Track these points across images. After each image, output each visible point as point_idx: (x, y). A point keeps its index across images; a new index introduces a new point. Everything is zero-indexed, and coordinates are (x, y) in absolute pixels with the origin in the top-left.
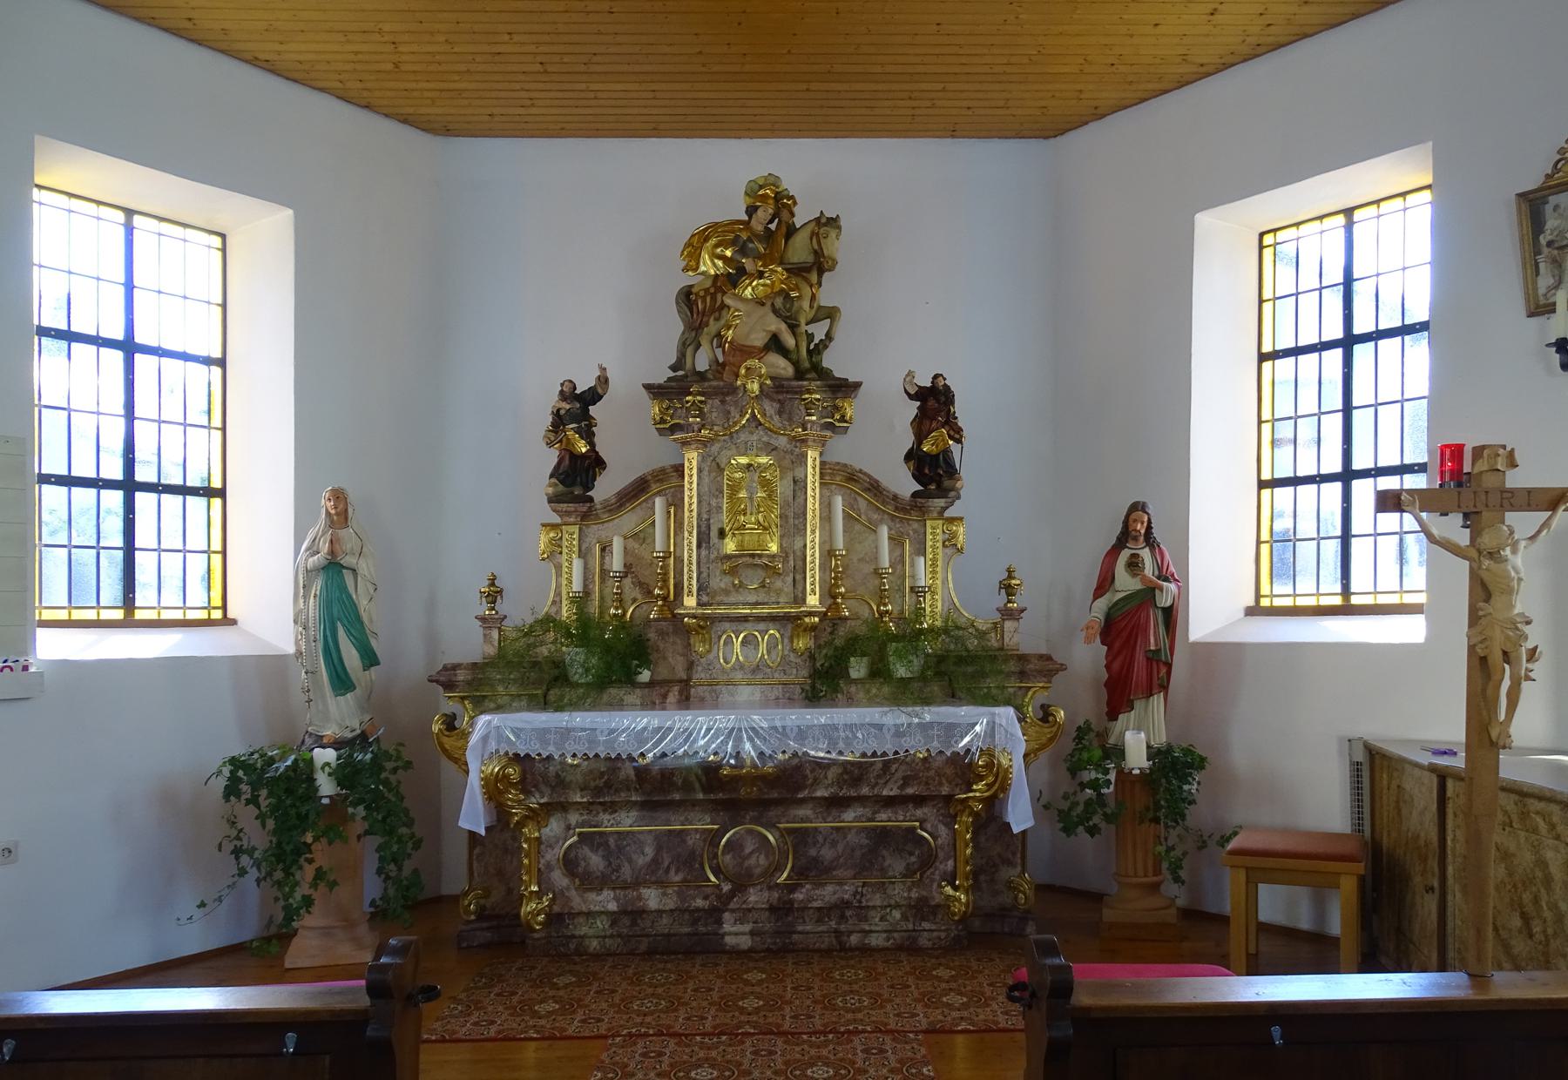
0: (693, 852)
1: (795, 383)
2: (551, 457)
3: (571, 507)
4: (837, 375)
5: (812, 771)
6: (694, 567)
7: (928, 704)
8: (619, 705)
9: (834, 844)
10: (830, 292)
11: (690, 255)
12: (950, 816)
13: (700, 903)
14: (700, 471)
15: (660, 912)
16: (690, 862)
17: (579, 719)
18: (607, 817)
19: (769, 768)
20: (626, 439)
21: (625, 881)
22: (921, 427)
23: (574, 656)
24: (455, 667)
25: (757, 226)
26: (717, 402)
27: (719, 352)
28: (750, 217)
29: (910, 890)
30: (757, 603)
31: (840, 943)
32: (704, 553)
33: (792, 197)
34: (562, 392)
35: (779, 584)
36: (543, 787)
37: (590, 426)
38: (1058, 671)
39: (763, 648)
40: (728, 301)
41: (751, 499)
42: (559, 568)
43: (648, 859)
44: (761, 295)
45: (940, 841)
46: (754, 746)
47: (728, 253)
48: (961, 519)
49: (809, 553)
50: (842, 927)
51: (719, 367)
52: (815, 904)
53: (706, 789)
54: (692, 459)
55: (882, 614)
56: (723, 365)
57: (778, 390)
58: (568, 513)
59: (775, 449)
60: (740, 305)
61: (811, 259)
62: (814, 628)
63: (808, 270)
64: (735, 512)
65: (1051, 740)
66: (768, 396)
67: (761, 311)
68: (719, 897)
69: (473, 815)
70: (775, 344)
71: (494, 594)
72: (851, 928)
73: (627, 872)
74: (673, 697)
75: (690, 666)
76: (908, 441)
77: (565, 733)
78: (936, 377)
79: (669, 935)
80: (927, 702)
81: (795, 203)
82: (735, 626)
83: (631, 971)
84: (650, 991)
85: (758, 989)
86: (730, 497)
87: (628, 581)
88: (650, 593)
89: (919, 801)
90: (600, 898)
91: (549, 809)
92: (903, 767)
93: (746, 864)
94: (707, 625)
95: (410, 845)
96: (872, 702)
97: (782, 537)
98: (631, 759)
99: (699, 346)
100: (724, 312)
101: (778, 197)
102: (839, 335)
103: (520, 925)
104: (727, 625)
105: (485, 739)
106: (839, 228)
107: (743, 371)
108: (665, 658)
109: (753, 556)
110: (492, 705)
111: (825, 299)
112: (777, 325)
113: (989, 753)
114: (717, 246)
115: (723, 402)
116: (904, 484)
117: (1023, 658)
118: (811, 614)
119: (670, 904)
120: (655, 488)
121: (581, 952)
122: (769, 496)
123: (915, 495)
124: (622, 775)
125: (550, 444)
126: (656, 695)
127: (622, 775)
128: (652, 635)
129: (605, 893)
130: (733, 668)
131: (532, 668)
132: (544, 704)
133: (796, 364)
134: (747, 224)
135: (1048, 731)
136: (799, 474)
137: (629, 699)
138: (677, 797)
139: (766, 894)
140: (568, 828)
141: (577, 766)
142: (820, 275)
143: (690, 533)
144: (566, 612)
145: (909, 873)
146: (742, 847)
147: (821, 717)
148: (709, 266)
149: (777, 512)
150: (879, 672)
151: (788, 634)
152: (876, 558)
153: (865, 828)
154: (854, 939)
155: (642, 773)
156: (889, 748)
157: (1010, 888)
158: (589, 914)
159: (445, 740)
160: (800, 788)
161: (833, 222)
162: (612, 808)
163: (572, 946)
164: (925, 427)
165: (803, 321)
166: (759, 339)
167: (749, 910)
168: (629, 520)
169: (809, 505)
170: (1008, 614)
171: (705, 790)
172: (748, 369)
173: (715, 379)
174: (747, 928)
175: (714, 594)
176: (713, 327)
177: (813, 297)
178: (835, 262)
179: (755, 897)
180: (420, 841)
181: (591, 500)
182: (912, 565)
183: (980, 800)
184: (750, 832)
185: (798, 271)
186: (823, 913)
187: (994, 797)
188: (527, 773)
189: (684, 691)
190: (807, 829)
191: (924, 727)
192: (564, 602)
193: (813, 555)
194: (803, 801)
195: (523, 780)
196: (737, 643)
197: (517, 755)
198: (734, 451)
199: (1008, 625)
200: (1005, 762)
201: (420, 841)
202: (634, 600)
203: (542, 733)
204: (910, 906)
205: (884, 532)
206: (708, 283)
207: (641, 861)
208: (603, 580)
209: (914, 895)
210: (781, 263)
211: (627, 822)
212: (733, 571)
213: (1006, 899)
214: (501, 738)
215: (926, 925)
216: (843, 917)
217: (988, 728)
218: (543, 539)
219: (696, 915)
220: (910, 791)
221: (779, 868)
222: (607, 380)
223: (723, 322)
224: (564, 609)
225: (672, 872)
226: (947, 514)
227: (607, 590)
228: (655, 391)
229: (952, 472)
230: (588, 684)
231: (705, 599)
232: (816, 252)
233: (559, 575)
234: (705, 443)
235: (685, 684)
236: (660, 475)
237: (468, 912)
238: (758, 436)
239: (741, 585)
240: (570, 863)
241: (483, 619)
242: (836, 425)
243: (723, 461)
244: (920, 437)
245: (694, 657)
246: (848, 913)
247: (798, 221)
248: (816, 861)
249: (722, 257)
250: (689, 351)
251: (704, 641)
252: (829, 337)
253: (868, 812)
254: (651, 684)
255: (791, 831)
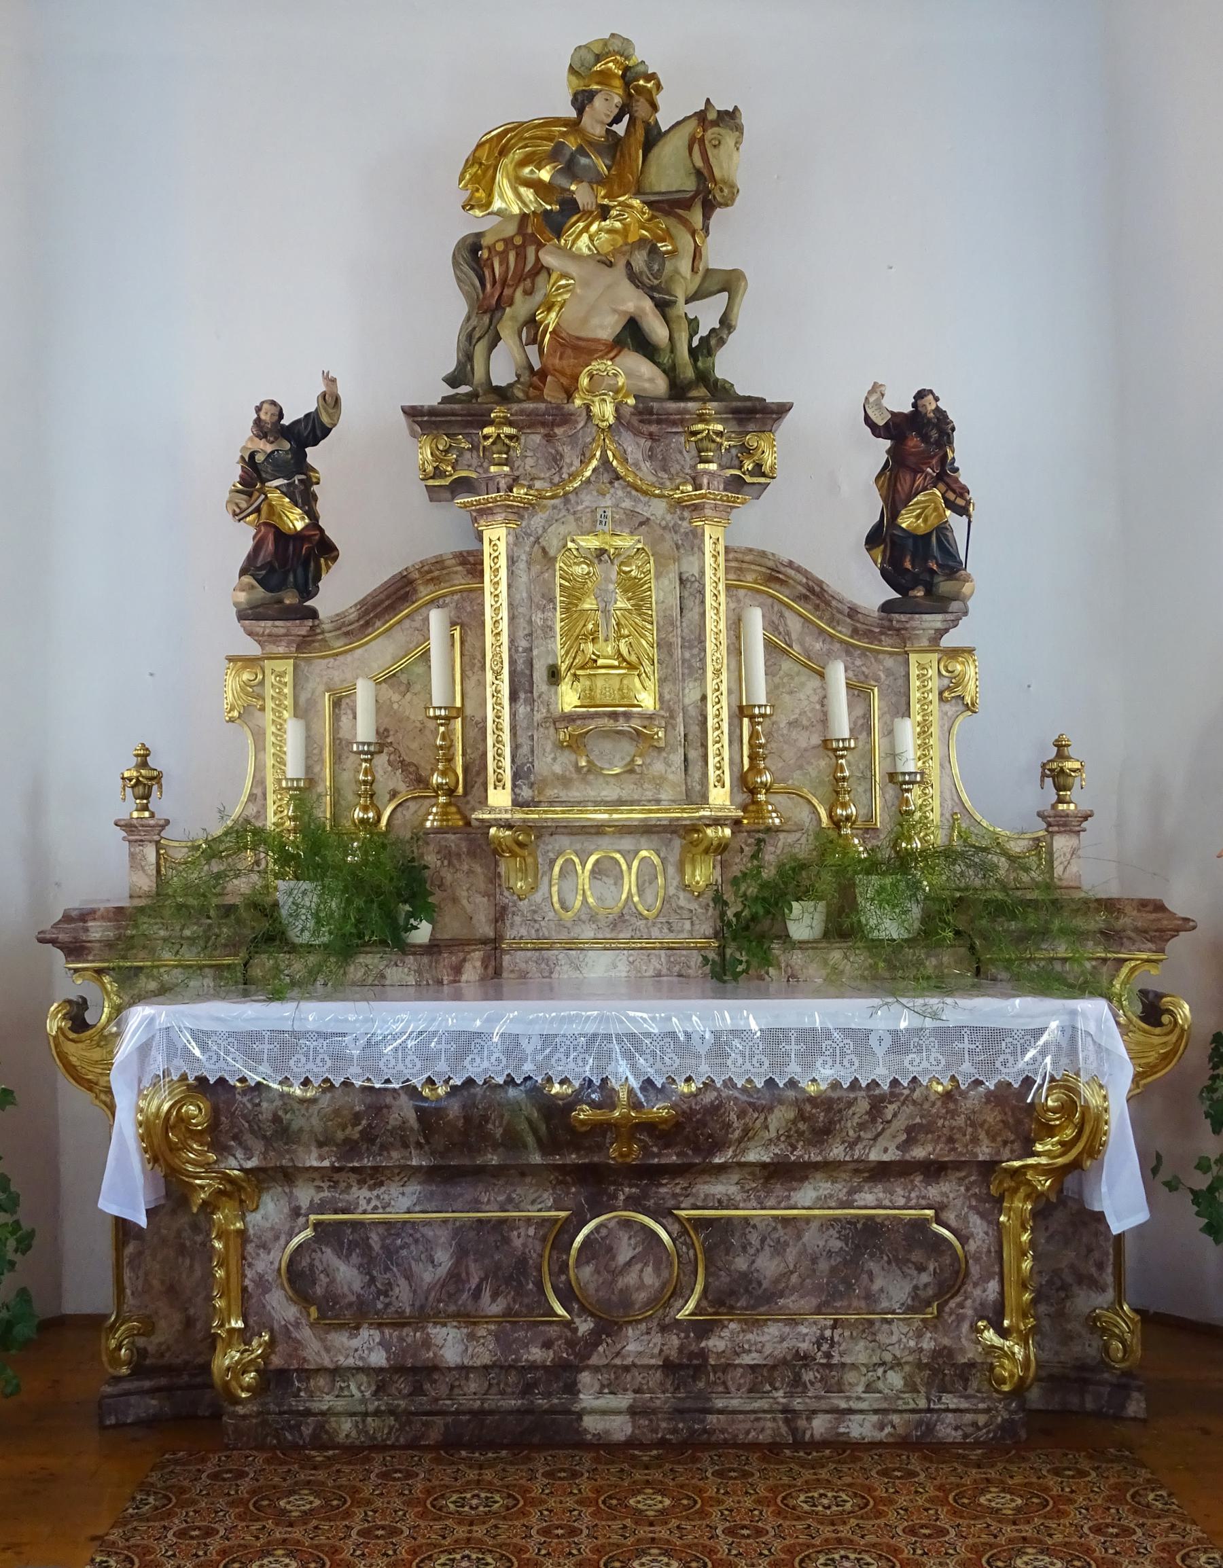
0: (522, 1261)
1: (672, 406)
2: (241, 540)
3: (280, 626)
4: (741, 392)
5: (742, 1114)
6: (506, 737)
7: (950, 993)
8: (376, 988)
9: (779, 1249)
10: (726, 241)
11: (475, 179)
12: (990, 1198)
13: (536, 1354)
14: (512, 561)
15: (464, 1369)
16: (515, 1276)
17: (314, 1014)
18: (365, 1193)
19: (659, 1109)
20: (373, 506)
21: (401, 1313)
22: (896, 482)
23: (298, 899)
24: (84, 916)
25: (594, 126)
26: (537, 438)
27: (532, 351)
28: (580, 111)
29: (919, 1335)
30: (621, 802)
31: (794, 1431)
32: (522, 710)
33: (651, 77)
34: (258, 422)
35: (658, 767)
36: (248, 1138)
37: (308, 483)
38: (1177, 931)
39: (630, 882)
40: (548, 259)
41: (605, 612)
42: (259, 736)
43: (442, 1271)
44: (607, 248)
45: (972, 1246)
46: (634, 1067)
47: (545, 175)
48: (970, 651)
49: (711, 711)
50: (797, 1403)
51: (536, 378)
52: (747, 1359)
53: (547, 1146)
54: (497, 538)
55: (837, 824)
56: (543, 374)
57: (644, 417)
58: (274, 638)
59: (646, 522)
60: (572, 268)
61: (690, 185)
62: (722, 848)
63: (687, 204)
64: (578, 636)
65: (1166, 1058)
66: (629, 427)
67: (608, 276)
68: (571, 1344)
69: (124, 1188)
70: (633, 336)
71: (145, 783)
72: (814, 1405)
73: (403, 1295)
74: (471, 972)
75: (500, 915)
76: (870, 509)
77: (287, 1042)
78: (921, 395)
79: (482, 1412)
80: (941, 985)
81: (659, 87)
82: (579, 842)
83: (419, 1486)
84: (461, 1532)
85: (662, 1532)
86: (567, 609)
87: (381, 760)
88: (421, 781)
89: (933, 1170)
90: (355, 1343)
91: (261, 1178)
92: (908, 1109)
93: (621, 1283)
94: (530, 838)
95: (12, 1243)
96: (835, 985)
97: (662, 681)
98: (412, 1091)
99: (497, 339)
100: (542, 277)
101: (629, 76)
102: (742, 319)
103: (211, 1386)
104: (564, 841)
105: (144, 1050)
106: (739, 128)
107: (584, 381)
108: (455, 900)
109: (614, 716)
110: (153, 985)
111: (718, 257)
112: (638, 303)
113: (1066, 1087)
114: (523, 163)
115: (549, 438)
116: (867, 588)
117: (1109, 906)
118: (717, 822)
119: (484, 1354)
120: (425, 593)
121: (324, 1439)
122: (638, 607)
123: (887, 607)
124: (394, 1119)
125: (239, 515)
126: (440, 967)
127: (394, 1119)
128: (431, 859)
129: (365, 1333)
130: (577, 920)
131: (219, 918)
132: (244, 984)
133: (670, 372)
134: (574, 125)
135: (1158, 1040)
136: (691, 569)
137: (394, 974)
138: (494, 1159)
139: (657, 1339)
140: (296, 1212)
141: (313, 1101)
142: (707, 216)
143: (497, 674)
144: (275, 814)
145: (917, 1304)
146: (610, 1251)
147: (749, 1015)
148: (509, 200)
149: (653, 637)
150: (842, 928)
151: (674, 857)
152: (824, 720)
153: (836, 1219)
154: (819, 1426)
155: (429, 1117)
156: (882, 1073)
157: (1093, 1329)
158: (336, 1372)
159: (70, 1048)
160: (718, 1145)
161: (729, 118)
162: (374, 1177)
163: (307, 1431)
164: (904, 487)
165: (681, 300)
166: (606, 327)
167: (627, 1369)
168: (381, 650)
169: (710, 625)
170: (1058, 823)
171: (543, 1148)
172: (591, 376)
173: (528, 399)
174: (623, 1401)
175: (544, 783)
176: (521, 306)
177: (697, 254)
178: (734, 192)
179: (638, 1345)
180: (31, 1234)
181: (313, 614)
182: (890, 733)
183: (1047, 1171)
184: (627, 1224)
185: (668, 206)
186: (762, 1376)
187: (1076, 1165)
188: (219, 1111)
189: (491, 958)
190: (729, 1219)
191: (947, 1036)
192: (271, 797)
193: (718, 713)
194: (723, 1168)
195: (214, 1125)
196: (584, 875)
197: (202, 1080)
198: (571, 526)
199: (1061, 843)
200: (1095, 1101)
201: (31, 1234)
202: (394, 794)
203: (247, 1041)
204: (920, 1366)
205: (838, 674)
206: (511, 230)
207: (428, 1276)
208: (337, 758)
209: (927, 1344)
210: (638, 193)
211: (400, 1202)
212: (575, 744)
213: (1089, 1348)
214: (172, 1050)
215: (950, 1401)
216: (797, 1384)
217: (1077, 1041)
218: (232, 684)
219: (530, 1379)
220: (919, 1153)
221: (679, 1292)
222: (337, 401)
223: (538, 297)
224: (271, 809)
225: (486, 1296)
226: (947, 641)
227: (346, 776)
228: (422, 419)
229: (953, 566)
230: (326, 946)
231: (526, 793)
232: (699, 173)
233: (260, 747)
234: (518, 512)
235: (494, 946)
236: (434, 571)
237: (115, 1361)
238: (612, 500)
239: (592, 768)
240: (299, 1278)
241: (128, 827)
242: (747, 481)
243: (552, 542)
244: (894, 503)
245: (506, 898)
246: (808, 1376)
247: (665, 120)
248: (747, 1281)
249: (537, 185)
250: (480, 349)
251: (524, 871)
252: (726, 323)
253: (839, 1189)
254: (433, 948)
255: (700, 1224)
